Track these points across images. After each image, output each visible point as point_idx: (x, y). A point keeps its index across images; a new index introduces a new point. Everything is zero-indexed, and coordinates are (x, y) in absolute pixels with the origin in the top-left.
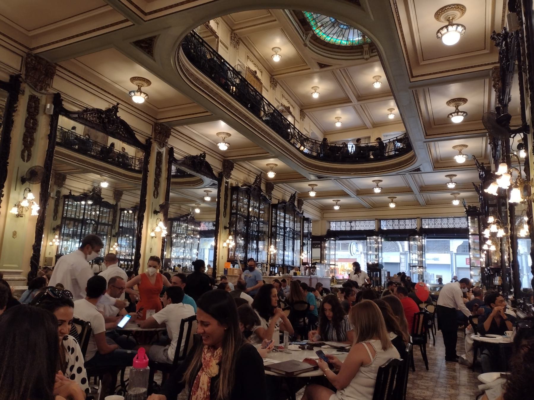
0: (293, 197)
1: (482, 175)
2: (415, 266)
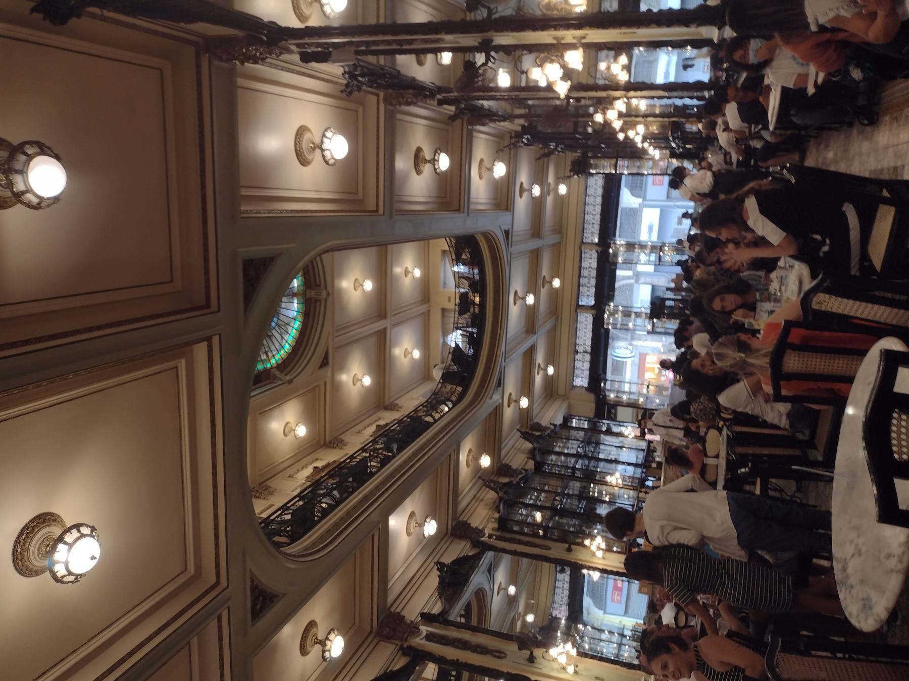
0: (526, 436)
1: (528, 139)
2: (660, 257)
